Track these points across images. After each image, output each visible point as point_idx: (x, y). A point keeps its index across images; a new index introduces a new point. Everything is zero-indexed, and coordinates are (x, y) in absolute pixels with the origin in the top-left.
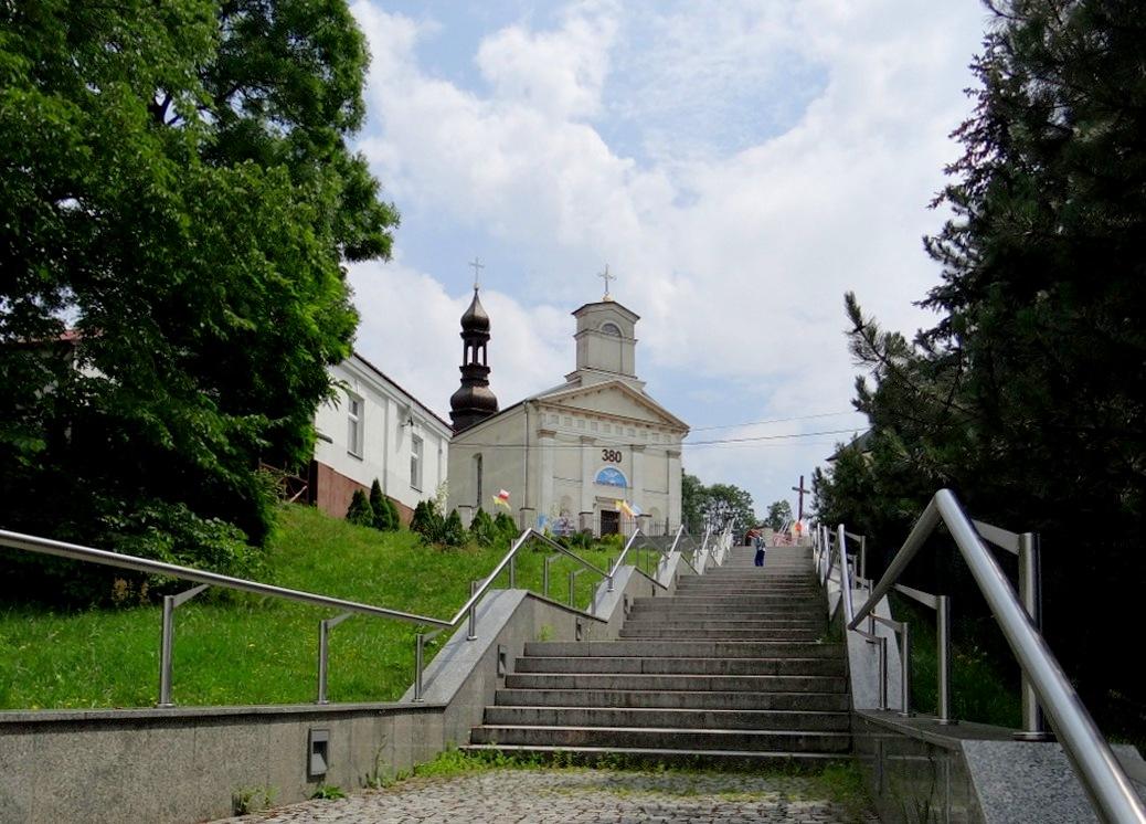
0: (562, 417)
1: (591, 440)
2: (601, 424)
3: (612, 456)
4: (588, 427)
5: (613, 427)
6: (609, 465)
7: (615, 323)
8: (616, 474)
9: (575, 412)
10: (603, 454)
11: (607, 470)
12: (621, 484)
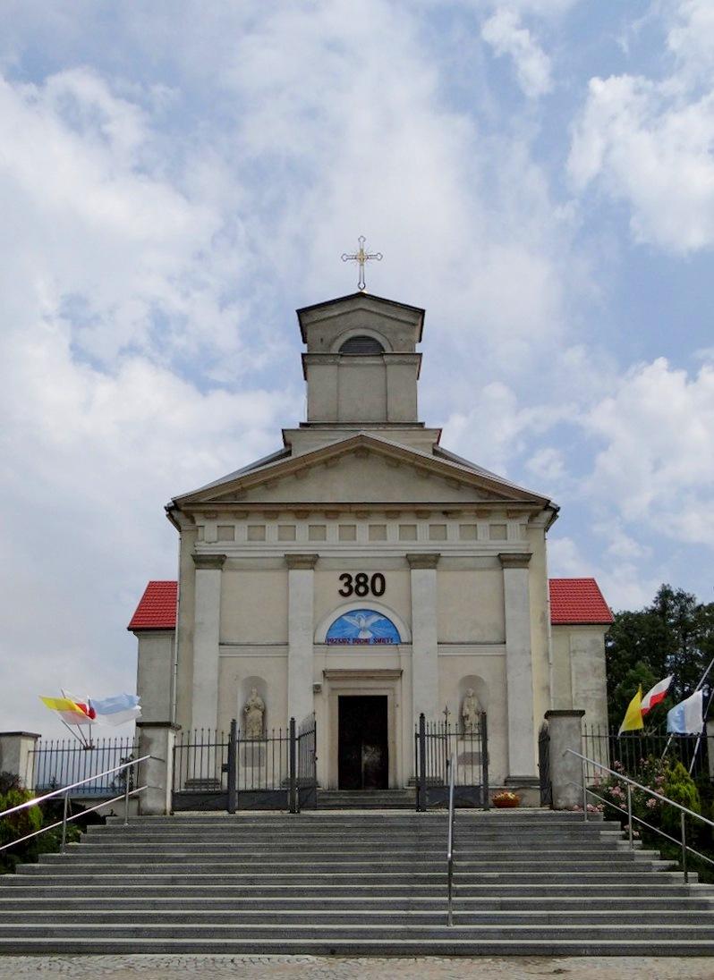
0: (241, 529)
1: (311, 562)
2: (333, 528)
3: (361, 585)
4: (302, 538)
5: (363, 529)
6: (355, 603)
7: (351, 334)
8: (375, 619)
9: (272, 511)
10: (341, 585)
11: (347, 614)
12: (387, 637)
